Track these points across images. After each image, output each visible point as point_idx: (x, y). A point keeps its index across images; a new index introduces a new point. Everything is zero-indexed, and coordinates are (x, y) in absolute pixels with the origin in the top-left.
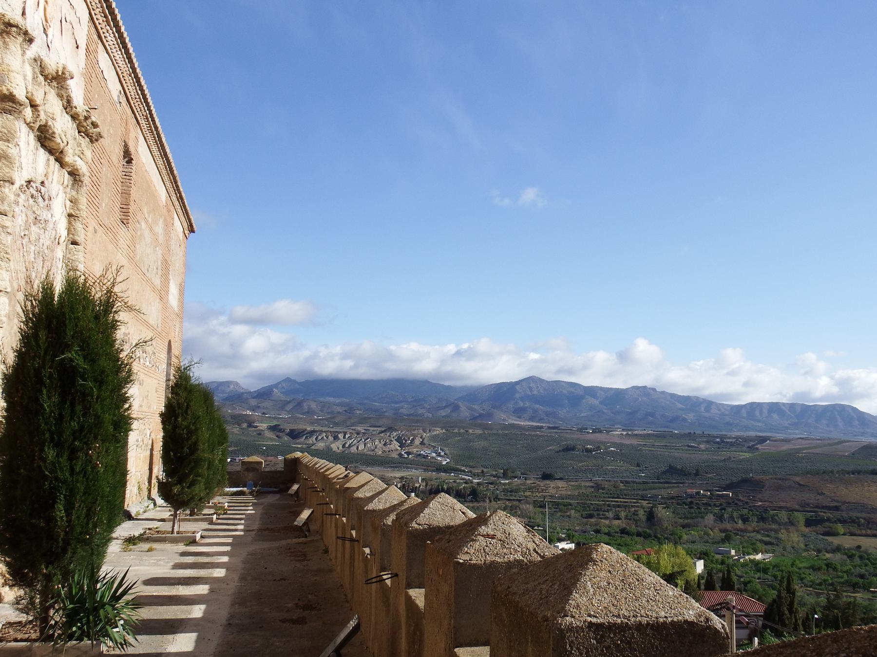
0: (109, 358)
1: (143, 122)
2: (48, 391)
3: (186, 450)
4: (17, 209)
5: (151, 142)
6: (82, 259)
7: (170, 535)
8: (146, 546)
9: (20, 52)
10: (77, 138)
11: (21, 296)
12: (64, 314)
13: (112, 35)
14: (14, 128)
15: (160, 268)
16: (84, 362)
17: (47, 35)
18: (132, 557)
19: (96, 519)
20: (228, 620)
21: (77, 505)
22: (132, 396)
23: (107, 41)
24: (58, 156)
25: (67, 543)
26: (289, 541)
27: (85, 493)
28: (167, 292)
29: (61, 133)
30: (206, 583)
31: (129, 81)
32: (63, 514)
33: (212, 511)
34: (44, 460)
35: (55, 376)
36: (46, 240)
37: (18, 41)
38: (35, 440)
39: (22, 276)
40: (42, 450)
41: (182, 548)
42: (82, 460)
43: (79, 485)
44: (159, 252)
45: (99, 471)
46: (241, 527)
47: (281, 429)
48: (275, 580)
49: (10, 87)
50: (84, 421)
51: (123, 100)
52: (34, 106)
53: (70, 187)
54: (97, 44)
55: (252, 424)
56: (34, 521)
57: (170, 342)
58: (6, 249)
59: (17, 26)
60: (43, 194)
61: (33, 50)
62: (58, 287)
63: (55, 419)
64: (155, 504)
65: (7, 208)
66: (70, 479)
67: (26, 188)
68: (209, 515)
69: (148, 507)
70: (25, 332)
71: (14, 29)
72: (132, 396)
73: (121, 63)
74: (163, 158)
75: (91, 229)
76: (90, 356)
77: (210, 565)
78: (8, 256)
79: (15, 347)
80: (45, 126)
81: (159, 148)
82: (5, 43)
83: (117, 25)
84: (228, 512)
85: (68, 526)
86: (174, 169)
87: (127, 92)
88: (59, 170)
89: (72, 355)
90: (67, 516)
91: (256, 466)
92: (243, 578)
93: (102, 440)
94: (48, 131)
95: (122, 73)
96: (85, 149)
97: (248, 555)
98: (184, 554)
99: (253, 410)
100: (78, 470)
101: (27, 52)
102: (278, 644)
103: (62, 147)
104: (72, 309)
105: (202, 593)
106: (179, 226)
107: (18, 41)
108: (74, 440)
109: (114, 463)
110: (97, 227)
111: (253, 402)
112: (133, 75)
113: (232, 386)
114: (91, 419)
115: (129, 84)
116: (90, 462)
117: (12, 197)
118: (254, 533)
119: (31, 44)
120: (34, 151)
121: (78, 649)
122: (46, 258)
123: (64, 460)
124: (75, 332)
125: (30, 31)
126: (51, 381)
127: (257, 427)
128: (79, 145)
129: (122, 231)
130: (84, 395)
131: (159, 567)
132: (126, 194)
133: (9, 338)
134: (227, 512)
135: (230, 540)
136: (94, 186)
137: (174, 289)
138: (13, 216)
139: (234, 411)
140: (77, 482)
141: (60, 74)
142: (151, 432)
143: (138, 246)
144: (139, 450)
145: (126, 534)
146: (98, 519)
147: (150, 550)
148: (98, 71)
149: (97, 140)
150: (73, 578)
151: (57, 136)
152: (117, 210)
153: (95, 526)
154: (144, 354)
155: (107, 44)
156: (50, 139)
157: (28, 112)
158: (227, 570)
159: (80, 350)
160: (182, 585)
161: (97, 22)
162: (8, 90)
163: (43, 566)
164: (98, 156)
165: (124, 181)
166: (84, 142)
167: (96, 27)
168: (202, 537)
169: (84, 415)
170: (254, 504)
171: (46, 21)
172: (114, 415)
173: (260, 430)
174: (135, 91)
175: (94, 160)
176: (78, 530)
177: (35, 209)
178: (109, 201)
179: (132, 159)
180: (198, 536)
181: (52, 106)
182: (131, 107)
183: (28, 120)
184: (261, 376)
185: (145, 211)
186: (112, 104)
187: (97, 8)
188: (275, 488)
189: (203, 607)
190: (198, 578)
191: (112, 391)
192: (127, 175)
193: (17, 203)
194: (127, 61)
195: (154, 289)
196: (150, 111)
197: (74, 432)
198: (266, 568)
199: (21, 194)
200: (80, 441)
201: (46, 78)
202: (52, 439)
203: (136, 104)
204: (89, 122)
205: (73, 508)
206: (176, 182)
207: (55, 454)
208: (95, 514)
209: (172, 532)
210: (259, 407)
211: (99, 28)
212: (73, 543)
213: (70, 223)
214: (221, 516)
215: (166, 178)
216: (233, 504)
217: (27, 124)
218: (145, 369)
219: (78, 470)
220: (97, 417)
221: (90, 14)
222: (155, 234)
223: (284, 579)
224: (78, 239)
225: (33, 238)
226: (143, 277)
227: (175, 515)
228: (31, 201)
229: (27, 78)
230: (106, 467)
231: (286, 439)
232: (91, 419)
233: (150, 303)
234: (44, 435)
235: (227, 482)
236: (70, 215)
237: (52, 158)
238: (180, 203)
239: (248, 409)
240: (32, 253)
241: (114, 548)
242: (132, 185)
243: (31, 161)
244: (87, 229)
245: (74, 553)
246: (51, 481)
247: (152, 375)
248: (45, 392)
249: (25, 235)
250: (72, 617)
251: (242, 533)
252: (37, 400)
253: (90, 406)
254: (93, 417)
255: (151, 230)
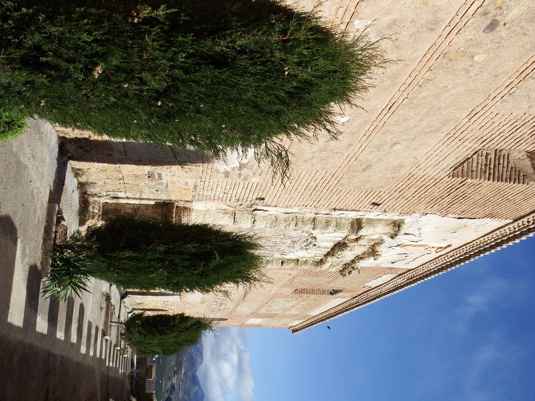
0: (216, 279)
1: (355, 301)
2: (197, 246)
3: (161, 328)
4: (299, 232)
5: (344, 306)
6: (273, 267)
7: (110, 320)
8: (104, 305)
9: (385, 232)
10: (342, 263)
11: (251, 234)
12: (241, 254)
13: (402, 282)
14: (343, 229)
15: (270, 312)
16: (214, 266)
17: (396, 246)
18: (98, 298)
19: (122, 273)
20: (53, 354)
21: (131, 263)
22: (194, 292)
23: (398, 279)
24: (331, 253)
25: (110, 258)
26: (99, 395)
27: (137, 267)
28: (256, 317)
29: (344, 254)
30: (77, 341)
31: (377, 292)
32: (127, 255)
33: (122, 347)
34: (158, 245)
35: (206, 250)
36: (283, 247)
37: (391, 231)
38: (170, 240)
39: (263, 235)
40: (164, 244)
41: (101, 327)
42: (157, 265)
43: (143, 264)
44: (280, 312)
45: (150, 275)
46: (111, 365)
47: (172, 392)
48: (75, 385)
49: (365, 227)
50: (180, 266)
51: (366, 289)
52: (357, 240)
53: (314, 260)
54: (396, 273)
55: (176, 374)
56: (123, 240)
57: (227, 320)
58: (277, 226)
59: (399, 230)
60: (309, 245)
61: (387, 239)
62: (257, 252)
63: (181, 250)
64: (129, 313)
65: (299, 227)
66: (146, 259)
67: (311, 236)
68: (120, 345)
69: (128, 308)
70: (230, 235)
71: (397, 229)
72: (194, 292)
73: (387, 287)
74: (335, 313)
75: (291, 272)
76: (217, 269)
77: (88, 344)
78: (273, 227)
79: (222, 229)
80: (347, 246)
81: (340, 310)
82: (389, 224)
83: (407, 284)
84: (121, 356)
85: (119, 258)
86: (329, 320)
87: (371, 291)
88: (323, 254)
89: (218, 259)
90: (125, 258)
91: (149, 375)
92: (78, 364)
93: (168, 276)
94: (344, 247)
95: (381, 288)
96: (336, 268)
97: (93, 368)
98: (97, 329)
99: (185, 374)
100: (151, 263)
101: (386, 236)
102: (33, 384)
103: (336, 255)
104: (244, 259)
105: (72, 338)
106: (296, 323)
107: (391, 231)
108: (169, 261)
109: (155, 283)
110: (292, 275)
111: (189, 374)
112: (381, 294)
113: (200, 360)
114: (181, 270)
115: (375, 292)
116: (156, 270)
117: (306, 229)
118: (107, 373)
119: (390, 237)
120: (332, 241)
121: (47, 265)
122: (273, 247)
123: (158, 255)
124: (231, 261)
125: (397, 237)
126: (203, 248)
127: (174, 376)
128: (338, 265)
129: (290, 290)
130: (195, 266)
131: (90, 313)
132: (312, 292)
133: (228, 229)
134: (121, 355)
135: (103, 357)
136: (315, 274)
137: (258, 321)
138: (295, 230)
139: (184, 361)
140: (145, 263)
141: (376, 253)
142: (172, 309)
143: (282, 299)
144: (162, 303)
145: (112, 295)
146: (122, 275)
147: (101, 308)
148: (381, 275)
149: (341, 274)
150: (89, 261)
151: (342, 252)
152: (303, 287)
153: (118, 273)
154: (219, 304)
155: (396, 279)
156: (339, 249)
157: (353, 237)
158: (85, 355)
159: (221, 263)
160: (78, 326)
161: (408, 273)
162: (364, 226)
163: (97, 245)
164: (333, 275)
165: (320, 290)
166: (340, 267)
167: (405, 273)
168: (107, 340)
169: (183, 266)
170: (125, 373)
171: (404, 246)
172: (182, 283)
173: (172, 378)
174: (372, 295)
175: (330, 273)
176: (116, 264)
177: (300, 241)
178: (308, 282)
179: (333, 295)
180: (107, 337)
181: (358, 250)
182: (362, 294)
183: (348, 237)
184: (206, 375)
185: (303, 303)
186: (363, 283)
187: (416, 273)
188: (135, 387)
189: (63, 338)
190: (81, 336)
191: (197, 282)
192: (323, 292)
193: (303, 232)
194: (388, 290)
195: (258, 309)
196: (361, 305)
197: (173, 261)
198: (83, 379)
199: (308, 234)
200: (168, 264)
201: (373, 246)
202: (170, 249)
203: (364, 296)
204: (351, 269)
205: (129, 261)
206: (322, 321)
207: (161, 250)
208: (125, 273)
209: (111, 322)
210: (187, 378)
211: (405, 275)
212: (109, 261)
213: (294, 260)
214: (119, 352)
215: (324, 315)
216: (126, 360)
217: (346, 237)
218: (210, 305)
219: (151, 263)
220: (182, 273)
221: (412, 270)
222: (290, 309)
223: (75, 391)
224: (285, 265)
225: (284, 240)
226: (265, 302)
227: (121, 323)
228: (305, 239)
229: (372, 236)
230: (152, 279)
231: (166, 396)
232: (181, 270)
233: (249, 307)
234: (173, 245)
235: (140, 356)
236: (298, 260)
237: (329, 250)
238: (310, 323)
239: (185, 371)
240: (275, 240)
241: (104, 286)
242: (318, 295)
243: (327, 239)
244: (291, 270)
245: (103, 262)
246: (146, 249)
247: (207, 309)
248: (197, 245)
249: (285, 236)
250: (66, 261)
251: (107, 365)
252: (193, 241)
253: (188, 269)
254: (181, 271)
255: (293, 307)
